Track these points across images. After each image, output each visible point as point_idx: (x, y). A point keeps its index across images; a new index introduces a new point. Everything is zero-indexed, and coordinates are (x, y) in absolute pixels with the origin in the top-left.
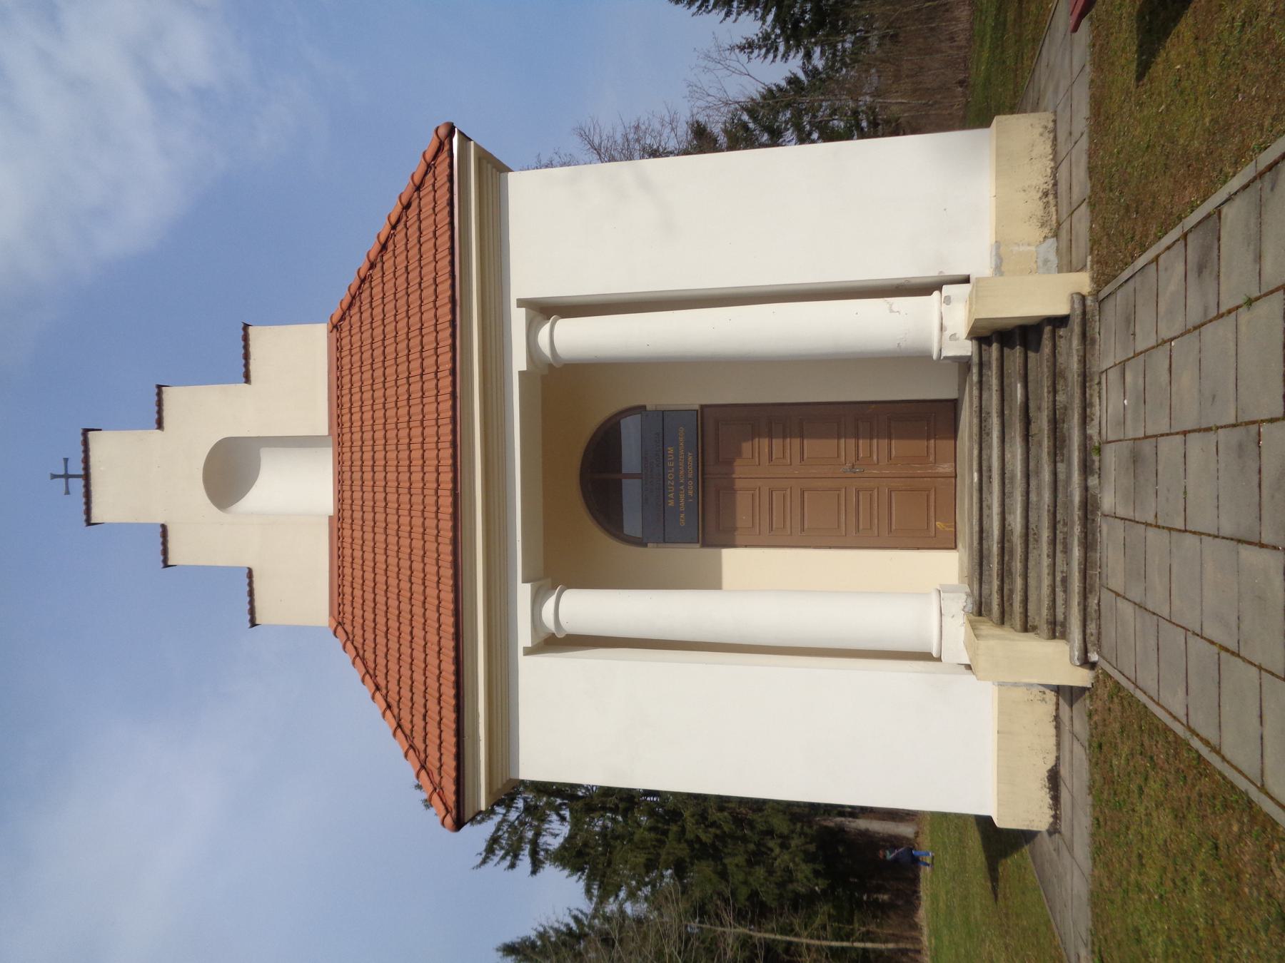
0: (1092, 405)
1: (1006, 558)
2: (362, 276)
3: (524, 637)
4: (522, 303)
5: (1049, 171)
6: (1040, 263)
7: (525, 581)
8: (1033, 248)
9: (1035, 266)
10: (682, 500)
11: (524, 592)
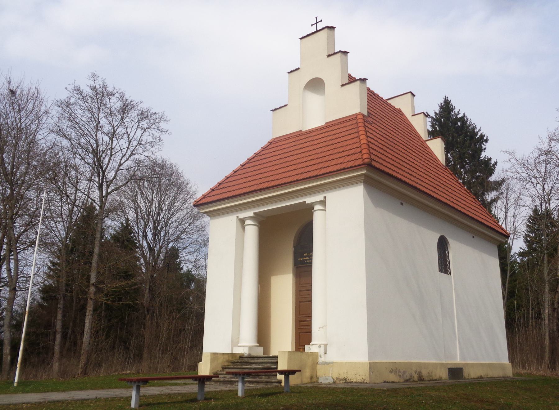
0: (252, 384)
1: (245, 364)
3: (242, 215)
4: (325, 197)
5: (352, 381)
6: (327, 377)
7: (254, 213)
8: (331, 375)
9: (326, 375)
10: (305, 258)
11: (250, 213)
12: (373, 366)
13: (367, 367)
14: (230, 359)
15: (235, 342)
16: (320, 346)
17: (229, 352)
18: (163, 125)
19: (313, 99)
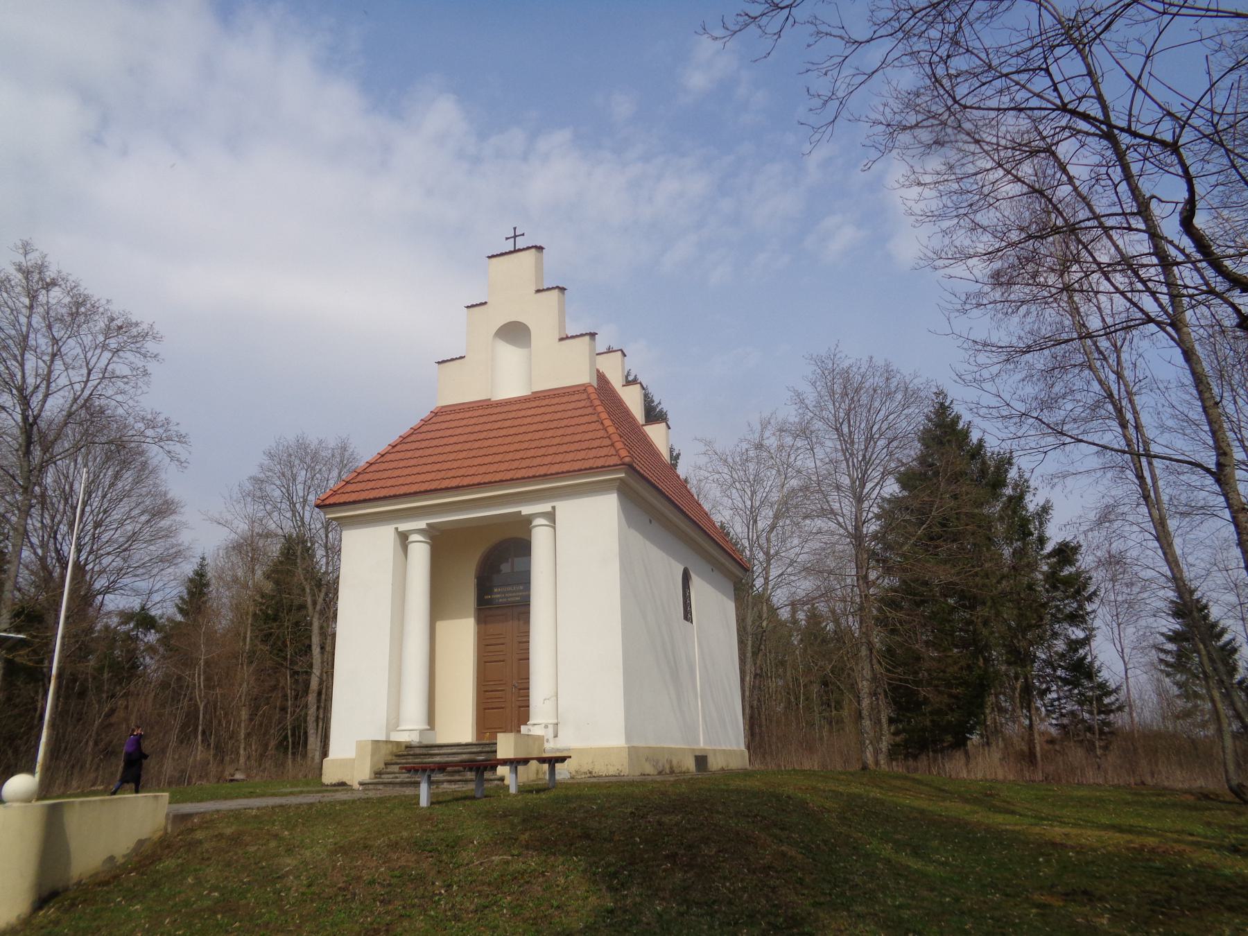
2: (830, 128)
3: (404, 526)
4: (554, 508)
11: (422, 524)
12: (633, 752)
13: (625, 754)
14: (395, 750)
15: (394, 721)
16: (546, 727)
17: (384, 739)
18: (150, 346)
19: (509, 354)
